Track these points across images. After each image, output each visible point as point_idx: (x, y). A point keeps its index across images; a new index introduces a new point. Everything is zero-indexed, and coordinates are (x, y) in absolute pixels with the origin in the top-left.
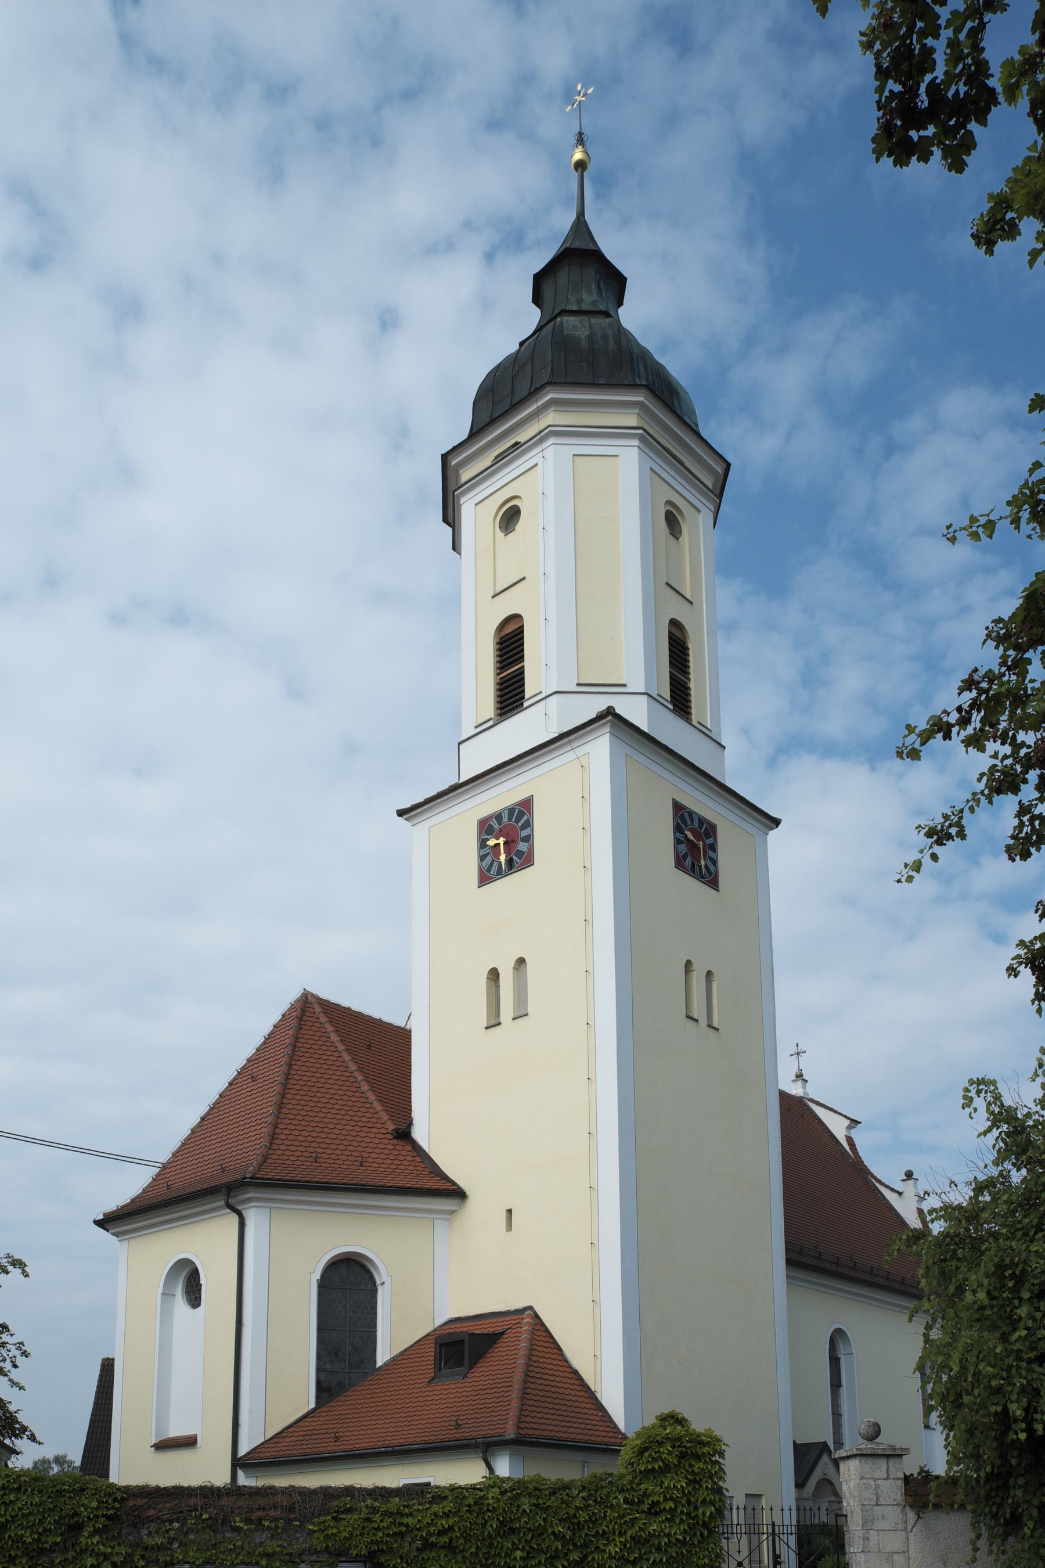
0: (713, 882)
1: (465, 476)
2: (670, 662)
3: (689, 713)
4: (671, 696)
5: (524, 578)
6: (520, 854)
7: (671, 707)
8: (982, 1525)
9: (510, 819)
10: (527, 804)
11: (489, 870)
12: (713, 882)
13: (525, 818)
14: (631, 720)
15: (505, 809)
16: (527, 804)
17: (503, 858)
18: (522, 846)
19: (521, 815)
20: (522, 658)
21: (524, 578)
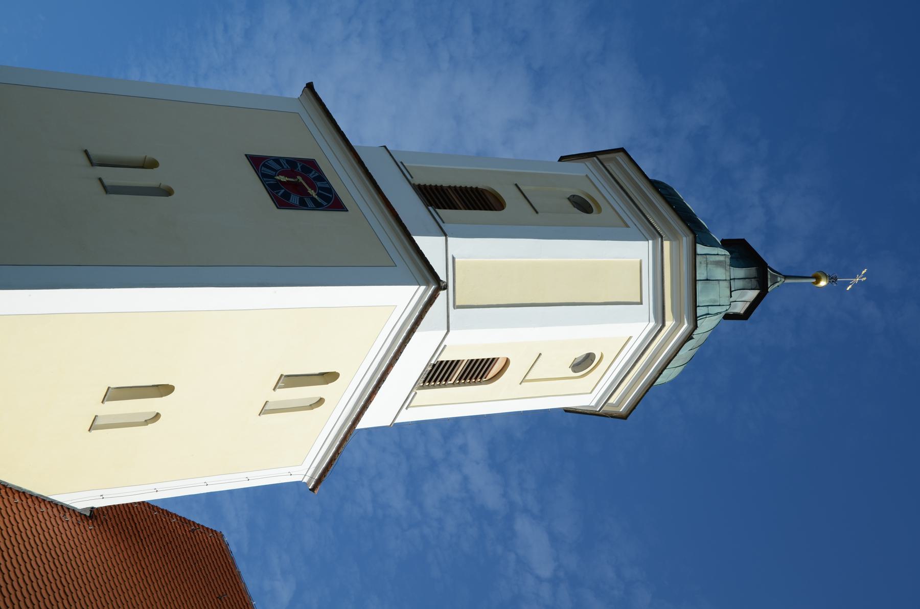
0: (256, 162)
1: (612, 167)
2: (472, 360)
3: (422, 388)
4: (442, 362)
5: (537, 212)
6: (287, 196)
7: (433, 362)
8: (546, 572)
9: (320, 188)
10: (337, 205)
11: (265, 166)
12: (256, 162)
13: (325, 203)
14: (408, 345)
15: (328, 183)
16: (337, 205)
17: (283, 178)
18: (295, 199)
19: (327, 199)
20: (468, 208)
21: (537, 212)
